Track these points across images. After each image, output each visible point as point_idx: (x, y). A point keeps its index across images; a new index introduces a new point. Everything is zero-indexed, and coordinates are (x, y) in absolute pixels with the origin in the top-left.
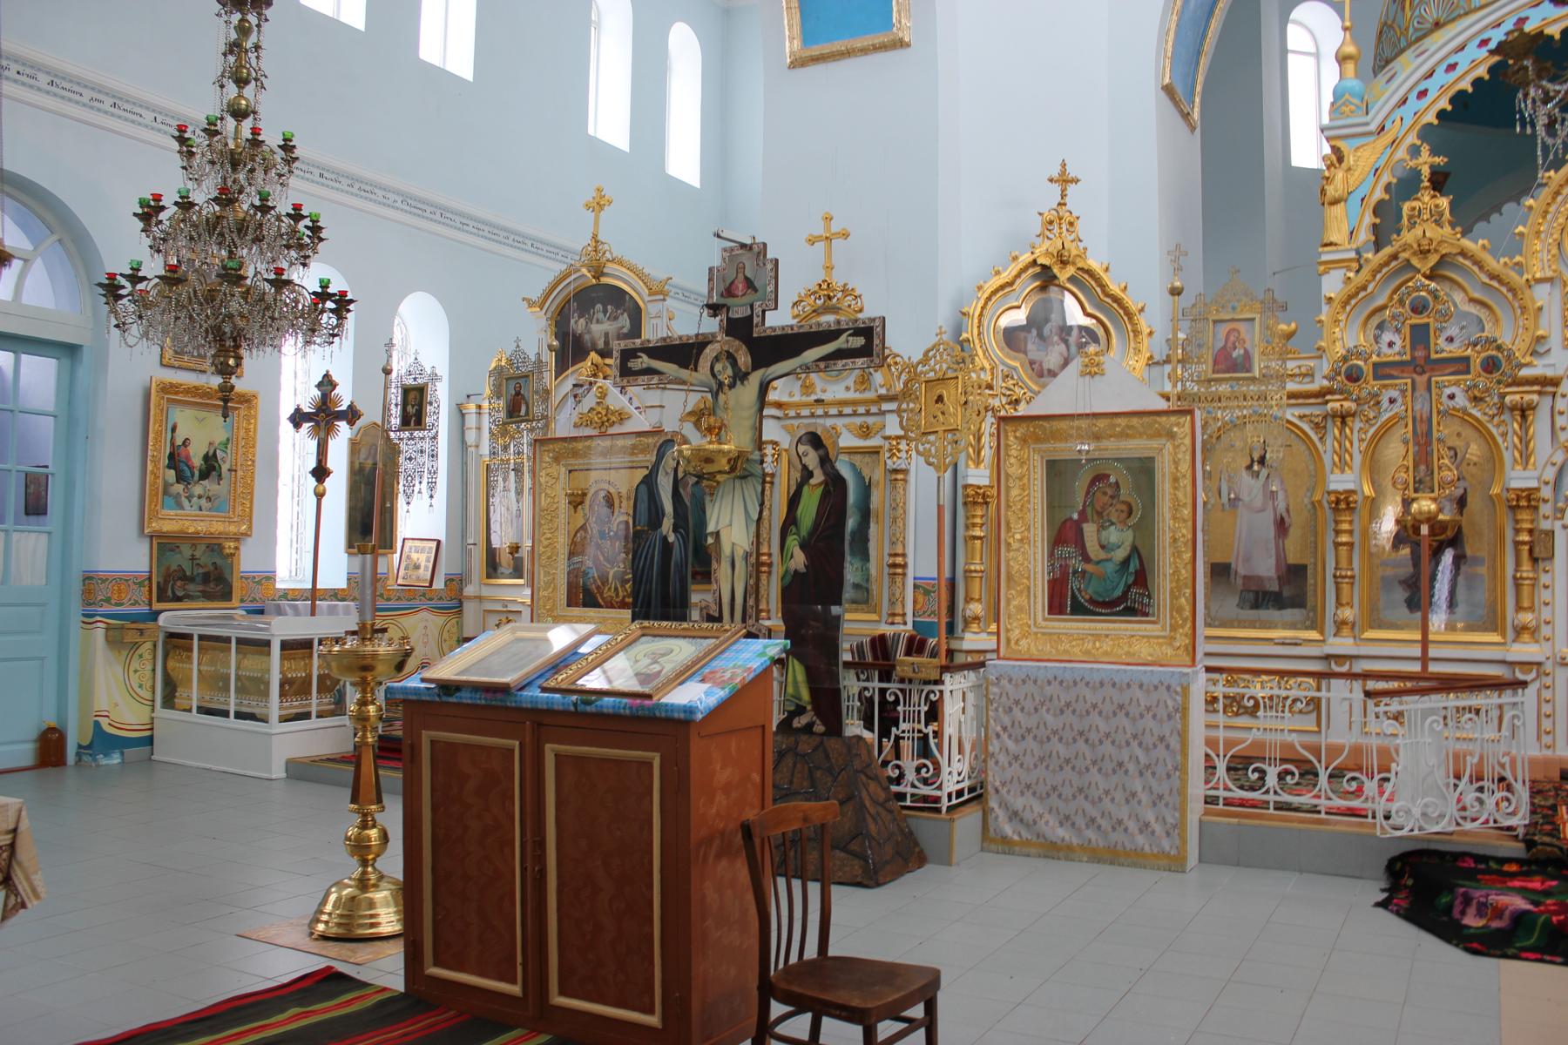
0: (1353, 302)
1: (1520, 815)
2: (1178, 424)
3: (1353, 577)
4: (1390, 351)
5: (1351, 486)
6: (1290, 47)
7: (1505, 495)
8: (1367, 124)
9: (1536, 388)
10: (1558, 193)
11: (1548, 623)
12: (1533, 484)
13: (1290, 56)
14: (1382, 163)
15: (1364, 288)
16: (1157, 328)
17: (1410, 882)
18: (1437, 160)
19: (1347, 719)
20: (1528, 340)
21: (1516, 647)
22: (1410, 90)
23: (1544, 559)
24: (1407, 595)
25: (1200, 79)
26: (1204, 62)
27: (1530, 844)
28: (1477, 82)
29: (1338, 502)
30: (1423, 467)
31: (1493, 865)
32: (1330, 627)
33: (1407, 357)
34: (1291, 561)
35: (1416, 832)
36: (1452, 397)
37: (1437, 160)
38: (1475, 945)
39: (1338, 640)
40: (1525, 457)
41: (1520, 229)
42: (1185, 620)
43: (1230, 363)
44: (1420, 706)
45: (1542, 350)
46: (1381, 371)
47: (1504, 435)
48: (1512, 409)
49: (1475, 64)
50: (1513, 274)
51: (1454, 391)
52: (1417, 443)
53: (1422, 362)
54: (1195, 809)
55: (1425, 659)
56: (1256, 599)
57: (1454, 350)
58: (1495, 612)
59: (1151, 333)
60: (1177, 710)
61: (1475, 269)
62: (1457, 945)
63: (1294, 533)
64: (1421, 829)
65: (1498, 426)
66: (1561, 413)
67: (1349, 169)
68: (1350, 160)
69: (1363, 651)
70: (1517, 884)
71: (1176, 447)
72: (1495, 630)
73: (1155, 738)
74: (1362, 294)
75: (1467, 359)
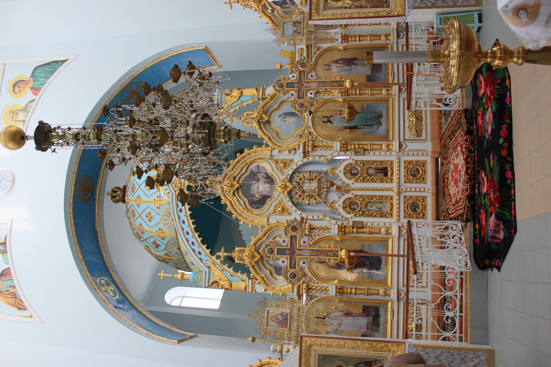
0: (267, 282)
1: (457, 224)
2: (306, 343)
3: (368, 289)
4: (286, 262)
5: (334, 287)
6: (178, 305)
7: (340, 236)
8: (206, 272)
10: (240, 215)
11: (385, 224)
12: (337, 226)
13: (182, 305)
14: (220, 268)
15: (263, 278)
16: (268, 356)
17: (487, 261)
18: (222, 250)
19: (423, 293)
21: (393, 234)
22: (197, 257)
23: (363, 224)
25: (179, 331)
26: (173, 329)
27: (467, 220)
28: (199, 236)
29: (340, 292)
30: (329, 254)
31: (477, 233)
32: (386, 298)
33: (289, 256)
34: (361, 312)
35: (468, 257)
36: (304, 242)
37: (222, 250)
38: (513, 231)
39: (392, 295)
40: (327, 229)
41: (250, 226)
42: (386, 346)
43: (284, 321)
44: (419, 255)
46: (293, 266)
47: (319, 235)
48: (310, 232)
49: (194, 236)
50: (265, 229)
51: (303, 241)
52: (320, 255)
53: (291, 251)
54: (464, 345)
55: (398, 256)
56: (376, 325)
57: (288, 240)
58: (381, 241)
59: (270, 358)
60: (424, 350)
61: (261, 241)
62: (514, 237)
63: (351, 310)
64: (466, 256)
65: (316, 237)
66: (313, 217)
67: (220, 279)
68: (217, 279)
70: (484, 222)
71: (315, 344)
73: (436, 360)
74: (265, 279)
75: (291, 236)
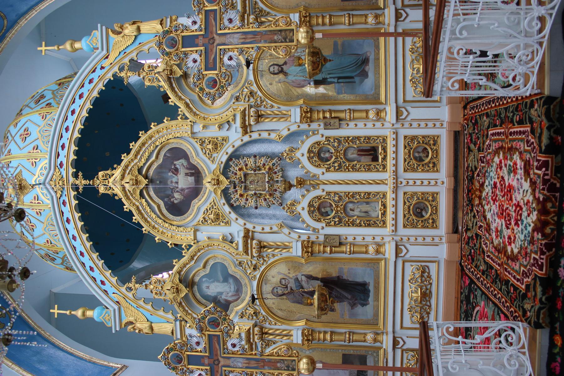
5: (300, 332)
8: (114, 310)
9: (249, 241)
11: (374, 238)
12: (299, 244)
20: (224, 245)
23: (340, 239)
24: (359, 306)
29: (308, 340)
30: (279, 365)
34: (341, 362)
45: (230, 238)
49: (92, 259)
52: (263, 367)
61: (188, 266)
69: (390, 329)
72: (379, 263)
